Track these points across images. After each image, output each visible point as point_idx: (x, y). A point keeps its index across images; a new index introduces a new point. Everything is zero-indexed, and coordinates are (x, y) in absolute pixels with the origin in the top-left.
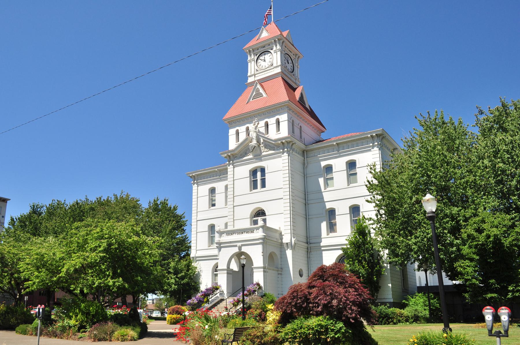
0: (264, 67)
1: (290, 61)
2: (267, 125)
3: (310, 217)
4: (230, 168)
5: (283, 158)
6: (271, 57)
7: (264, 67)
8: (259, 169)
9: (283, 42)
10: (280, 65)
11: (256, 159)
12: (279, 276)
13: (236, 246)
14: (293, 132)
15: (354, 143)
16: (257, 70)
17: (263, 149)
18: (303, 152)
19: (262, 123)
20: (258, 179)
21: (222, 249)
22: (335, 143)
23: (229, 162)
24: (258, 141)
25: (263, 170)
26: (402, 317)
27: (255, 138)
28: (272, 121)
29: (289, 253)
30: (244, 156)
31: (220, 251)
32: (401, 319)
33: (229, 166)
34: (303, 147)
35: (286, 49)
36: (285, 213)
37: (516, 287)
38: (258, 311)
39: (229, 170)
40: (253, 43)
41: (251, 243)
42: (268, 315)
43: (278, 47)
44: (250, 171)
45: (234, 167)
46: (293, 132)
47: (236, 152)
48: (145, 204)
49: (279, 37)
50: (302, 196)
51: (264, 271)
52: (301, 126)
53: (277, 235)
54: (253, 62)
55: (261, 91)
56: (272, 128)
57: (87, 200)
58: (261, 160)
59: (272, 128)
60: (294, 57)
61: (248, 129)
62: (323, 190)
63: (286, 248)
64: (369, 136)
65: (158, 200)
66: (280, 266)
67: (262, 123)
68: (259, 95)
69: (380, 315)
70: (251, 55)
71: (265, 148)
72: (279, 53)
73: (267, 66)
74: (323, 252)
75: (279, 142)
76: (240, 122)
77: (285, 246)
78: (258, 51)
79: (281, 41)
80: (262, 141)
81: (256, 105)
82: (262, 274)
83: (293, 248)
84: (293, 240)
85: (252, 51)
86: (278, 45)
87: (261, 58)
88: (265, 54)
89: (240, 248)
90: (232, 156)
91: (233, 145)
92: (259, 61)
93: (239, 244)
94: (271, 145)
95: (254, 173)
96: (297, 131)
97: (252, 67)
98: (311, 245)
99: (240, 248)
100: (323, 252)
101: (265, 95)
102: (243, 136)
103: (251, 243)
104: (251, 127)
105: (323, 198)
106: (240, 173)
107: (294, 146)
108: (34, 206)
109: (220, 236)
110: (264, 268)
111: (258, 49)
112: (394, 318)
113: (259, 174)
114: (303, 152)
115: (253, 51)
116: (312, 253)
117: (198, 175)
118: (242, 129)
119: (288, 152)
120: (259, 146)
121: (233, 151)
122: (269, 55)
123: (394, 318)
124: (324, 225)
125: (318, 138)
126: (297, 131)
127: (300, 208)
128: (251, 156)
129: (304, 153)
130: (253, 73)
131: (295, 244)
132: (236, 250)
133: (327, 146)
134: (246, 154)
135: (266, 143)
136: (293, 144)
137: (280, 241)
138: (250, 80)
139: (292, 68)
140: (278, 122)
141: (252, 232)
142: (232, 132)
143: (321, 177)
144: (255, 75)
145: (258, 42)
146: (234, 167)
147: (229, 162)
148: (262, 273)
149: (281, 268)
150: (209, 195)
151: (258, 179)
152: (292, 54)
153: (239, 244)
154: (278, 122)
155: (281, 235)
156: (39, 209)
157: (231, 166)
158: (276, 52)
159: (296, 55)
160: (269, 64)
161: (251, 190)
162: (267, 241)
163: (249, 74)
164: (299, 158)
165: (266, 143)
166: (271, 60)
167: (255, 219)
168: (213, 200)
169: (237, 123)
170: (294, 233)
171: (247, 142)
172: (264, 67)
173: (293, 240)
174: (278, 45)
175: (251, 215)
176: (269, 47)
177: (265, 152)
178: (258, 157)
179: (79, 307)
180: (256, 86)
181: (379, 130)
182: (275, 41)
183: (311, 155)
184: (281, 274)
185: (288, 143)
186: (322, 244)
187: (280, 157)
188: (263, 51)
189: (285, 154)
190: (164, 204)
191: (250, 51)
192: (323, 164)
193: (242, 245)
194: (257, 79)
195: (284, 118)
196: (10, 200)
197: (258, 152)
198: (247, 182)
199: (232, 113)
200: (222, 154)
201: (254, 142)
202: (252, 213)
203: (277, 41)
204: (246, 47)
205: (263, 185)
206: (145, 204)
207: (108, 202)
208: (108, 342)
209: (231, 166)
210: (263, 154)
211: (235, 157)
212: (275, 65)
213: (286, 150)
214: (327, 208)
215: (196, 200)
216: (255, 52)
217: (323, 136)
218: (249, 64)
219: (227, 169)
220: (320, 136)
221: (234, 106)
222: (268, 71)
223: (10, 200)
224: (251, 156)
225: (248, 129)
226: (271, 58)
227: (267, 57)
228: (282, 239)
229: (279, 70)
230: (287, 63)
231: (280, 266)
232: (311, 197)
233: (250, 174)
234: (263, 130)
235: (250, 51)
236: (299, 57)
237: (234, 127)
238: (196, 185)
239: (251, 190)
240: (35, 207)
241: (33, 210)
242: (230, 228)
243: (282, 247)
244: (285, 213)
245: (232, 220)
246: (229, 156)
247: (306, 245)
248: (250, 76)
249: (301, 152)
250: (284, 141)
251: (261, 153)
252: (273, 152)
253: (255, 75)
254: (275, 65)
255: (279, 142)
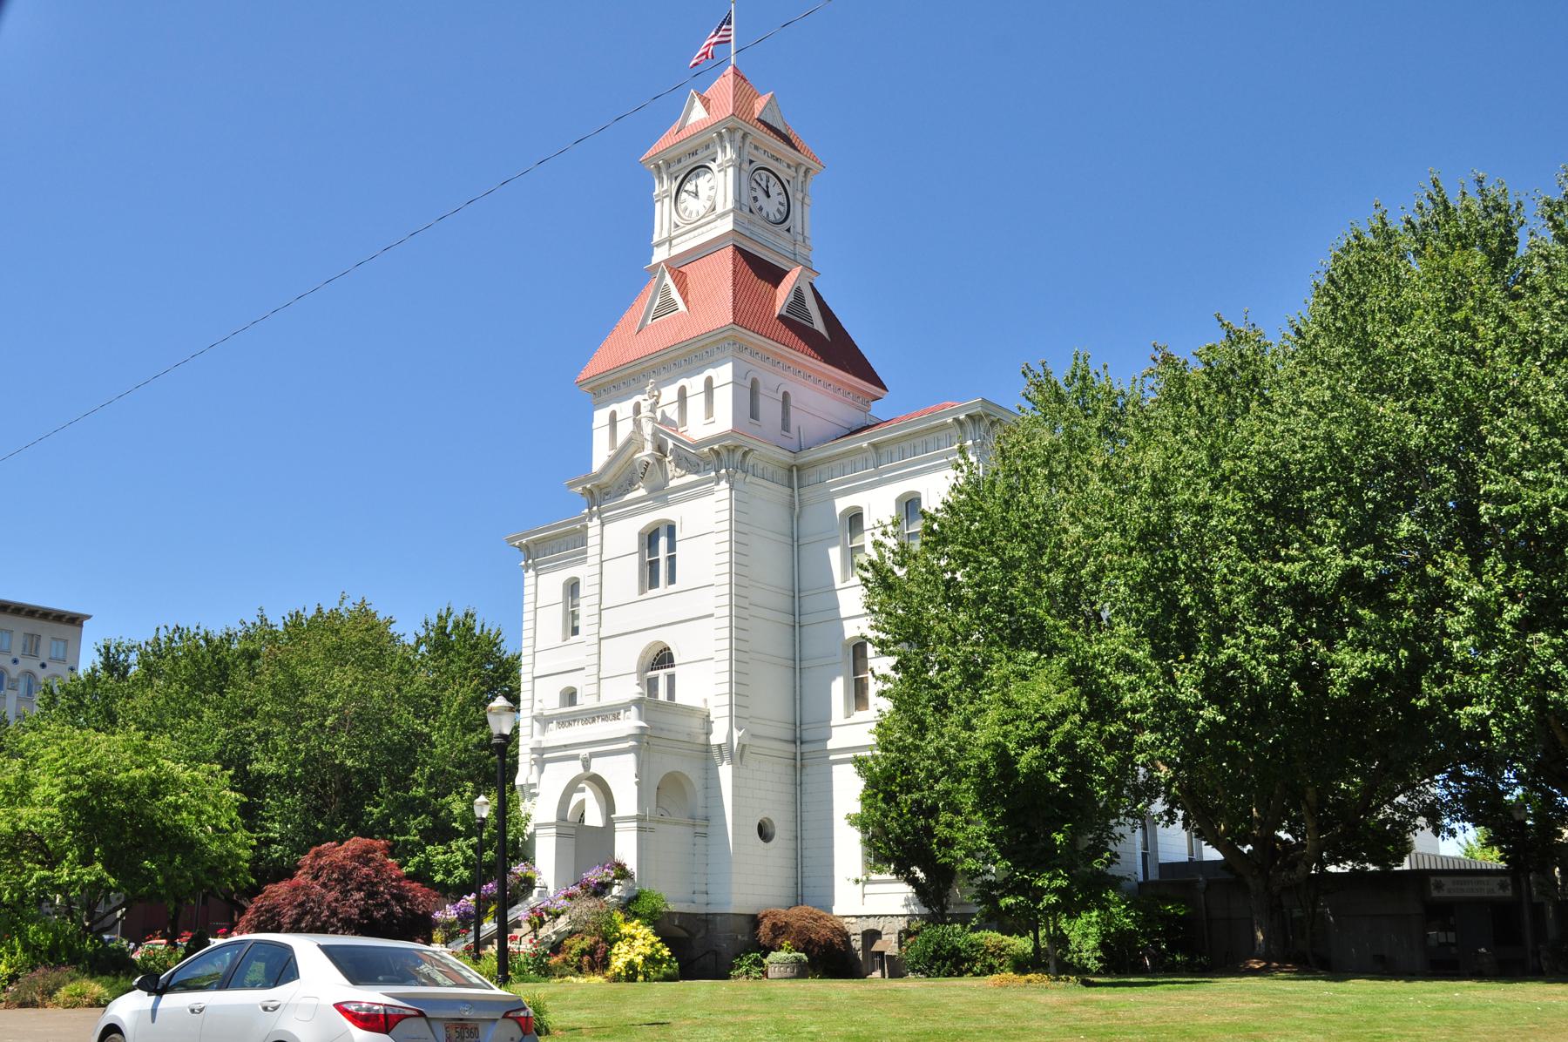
1: (775, 189)
2: (683, 395)
3: (805, 664)
4: (594, 526)
8: (663, 530)
9: (745, 136)
10: (733, 210)
12: (700, 840)
13: (575, 757)
14: (754, 414)
15: (845, 461)
17: (671, 467)
19: (669, 393)
20: (656, 556)
21: (548, 766)
22: (865, 445)
24: (660, 448)
25: (671, 530)
26: (1000, 956)
28: (695, 384)
29: (725, 772)
30: (628, 492)
31: (541, 771)
32: (996, 962)
34: (786, 457)
35: (759, 154)
36: (718, 656)
37: (1051, 880)
38: (588, 942)
41: (607, 749)
42: (615, 950)
43: (730, 153)
44: (641, 534)
45: (602, 524)
46: (754, 414)
47: (605, 479)
48: (408, 627)
50: (784, 602)
51: (640, 829)
52: (786, 395)
53: (696, 724)
54: (667, 200)
55: (675, 294)
56: (696, 404)
57: (263, 620)
58: (667, 504)
59: (696, 404)
60: (792, 172)
62: (838, 585)
63: (718, 760)
64: (950, 420)
65: (449, 614)
66: (700, 812)
68: (668, 305)
69: (935, 951)
70: (661, 181)
71: (677, 466)
72: (730, 171)
74: (835, 768)
77: (716, 752)
79: (739, 135)
80: (670, 445)
81: (662, 335)
82: (633, 835)
83: (739, 756)
84: (736, 734)
85: (663, 168)
87: (689, 187)
88: (698, 176)
89: (586, 764)
90: (596, 492)
91: (601, 454)
92: (684, 195)
93: (584, 752)
94: (692, 459)
95: (650, 539)
96: (770, 409)
97: (663, 214)
98: (806, 748)
99: (586, 764)
100: (835, 768)
101: (682, 307)
102: (625, 430)
103: (607, 749)
105: (837, 608)
106: (618, 537)
107: (750, 459)
108: (107, 648)
109: (544, 729)
110: (640, 819)
111: (679, 161)
112: (975, 960)
113: (663, 542)
114: (790, 470)
115: (668, 165)
116: (807, 770)
117: (535, 542)
118: (624, 409)
119: (729, 478)
120: (659, 461)
121: (598, 476)
122: (708, 176)
123: (975, 960)
124: (838, 688)
125: (858, 418)
126: (770, 409)
127: (771, 637)
128: (642, 492)
129: (795, 475)
130: (665, 235)
131: (743, 747)
132: (575, 768)
133: (850, 451)
134: (630, 485)
136: (745, 454)
137: (702, 739)
138: (660, 255)
139: (783, 209)
140: (709, 387)
141: (616, 717)
142: (601, 417)
143: (834, 545)
146: (602, 524)
147: (717, 472)
148: (635, 833)
149: (707, 819)
150: (565, 602)
151: (656, 556)
152: (783, 167)
153: (584, 752)
154: (709, 387)
155: (707, 721)
156: (122, 656)
158: (722, 169)
159: (798, 165)
160: (708, 204)
161: (642, 592)
162: (653, 741)
163: (656, 238)
164: (771, 496)
166: (712, 193)
167: (651, 674)
168: (575, 616)
170: (740, 712)
171: (632, 449)
173: (736, 734)
175: (640, 663)
176: (706, 153)
177: (678, 479)
178: (660, 494)
179: (22, 933)
180: (662, 277)
181: (973, 403)
182: (720, 134)
183: (813, 479)
184: (705, 835)
185: (731, 450)
186: (831, 745)
187: (711, 492)
188: (690, 167)
189: (724, 485)
190: (465, 628)
191: (658, 167)
192: (842, 504)
193: (592, 755)
194: (676, 251)
196: (89, 617)
197: (659, 478)
198: (630, 568)
199: (600, 362)
200: (571, 485)
201: (649, 448)
202: (642, 657)
203: (726, 137)
205: (672, 579)
206: (408, 627)
207: (335, 615)
208: (41, 1010)
210: (672, 484)
211: (604, 494)
212: (719, 210)
214: (847, 636)
215: (531, 616)
216: (672, 170)
217: (877, 410)
218: (658, 205)
223: (89, 617)
224: (642, 492)
227: (702, 183)
228: (708, 733)
229: (727, 225)
230: (760, 194)
231: (700, 812)
232: (809, 604)
233: (641, 545)
234: (673, 412)
235: (658, 167)
236: (807, 171)
237: (672, 381)
238: (531, 572)
239: (642, 592)
240: (113, 651)
241: (107, 658)
242: (585, 701)
243: (707, 756)
244: (718, 656)
245: (595, 679)
247: (791, 747)
248: (659, 245)
249: (782, 474)
254: (719, 210)
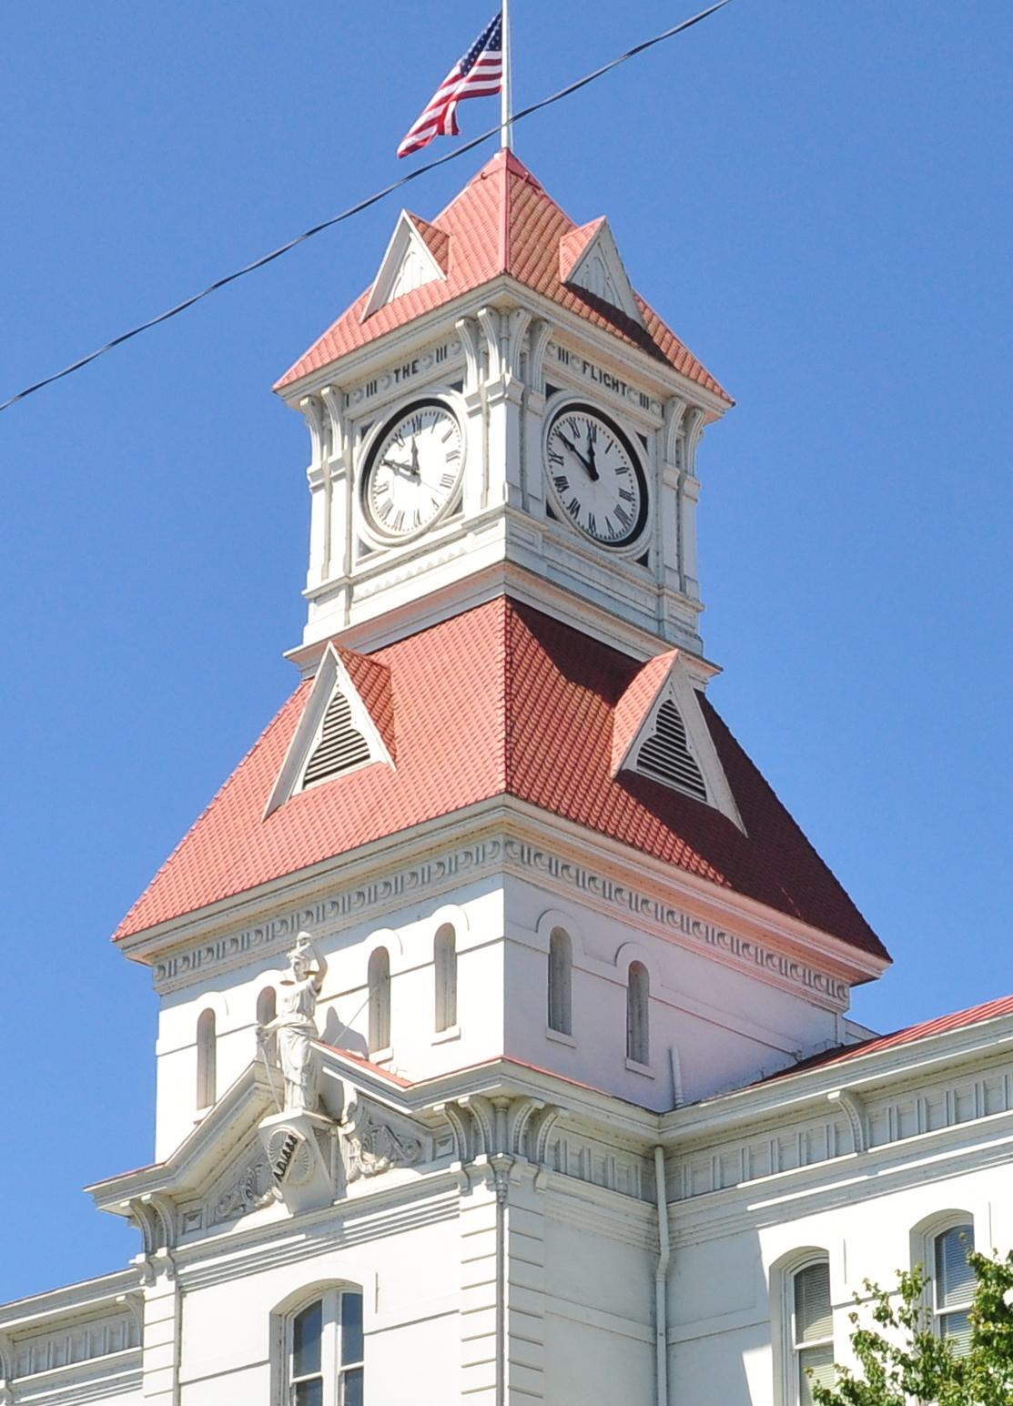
0: (409, 528)
1: (610, 458)
4: (158, 1297)
5: (467, 1221)
6: (452, 444)
7: (409, 522)
8: (332, 1307)
9: (535, 326)
11: (310, 1229)
14: (558, 1019)
15: (783, 1134)
16: (366, 550)
17: (350, 1151)
18: (649, 1158)
19: (347, 966)
22: (834, 1094)
23: (150, 1253)
24: (325, 1102)
25: (352, 1307)
27: (296, 1077)
28: (410, 944)
30: (244, 1210)
33: (151, 1282)
34: (638, 1126)
35: (571, 371)
39: (151, 1312)
40: (338, 340)
43: (498, 370)
44: (276, 1317)
45: (181, 1292)
46: (558, 1019)
47: (187, 1180)
49: (498, 298)
52: (636, 969)
54: (340, 487)
55: (361, 720)
56: (413, 993)
58: (340, 1240)
60: (652, 416)
61: (445, 938)
67: (347, 966)
68: (345, 748)
70: (327, 438)
71: (367, 1147)
72: (499, 413)
73: (428, 515)
75: (439, 1106)
76: (400, 887)
78: (374, 400)
79: (519, 324)
81: (327, 821)
85: (332, 404)
86: (494, 352)
88: (418, 426)
90: (164, 1211)
91: (176, 1119)
92: (382, 475)
96: (598, 1006)
97: (332, 520)
104: (283, 983)
111: (372, 388)
113: (331, 1335)
114: (649, 1158)
115: (344, 397)
118: (234, 1005)
119: (496, 1176)
120: (323, 1136)
121: (169, 1172)
122: (444, 426)
128: (278, 1212)
130: (337, 572)
134: (249, 1194)
135: (372, 1109)
136: (536, 1118)
138: (323, 623)
143: (760, 1343)
144: (349, 585)
145: (382, 323)
146: (181, 1292)
157: (165, 1284)
158: (479, 409)
159: (668, 400)
160: (444, 496)
163: (314, 581)
164: (601, 1220)
165: (372, 1109)
169: (208, 964)
171: (254, 1105)
172: (409, 522)
174: (494, 352)
177: (368, 1179)
178: (324, 1218)
180: (330, 678)
182: (473, 322)
183: (705, 1179)
185: (502, 1108)
189: (483, 1194)
191: (318, 403)
192: (776, 1242)
195: (481, 918)
197: (323, 1179)
201: (296, 1104)
203: (489, 328)
204: (296, 370)
209: (165, 1284)
210: (355, 1191)
211: (182, 1219)
212: (471, 510)
213: (481, 1160)
218: (319, 499)
219: (140, 1300)
220: (836, 1011)
221: (201, 831)
222: (433, 558)
224: (278, 1212)
225: (445, 938)
226: (452, 456)
227: (430, 442)
229: (490, 548)
233: (276, 1343)
236: (690, 413)
237: (352, 936)
246: (467, 1115)
248: (320, 597)
249: (627, 1165)
250: (463, 1100)
251: (340, 1184)
252: (404, 1176)
253: (349, 585)
254: (471, 510)
255: (439, 1106)
